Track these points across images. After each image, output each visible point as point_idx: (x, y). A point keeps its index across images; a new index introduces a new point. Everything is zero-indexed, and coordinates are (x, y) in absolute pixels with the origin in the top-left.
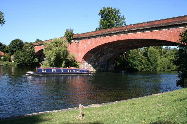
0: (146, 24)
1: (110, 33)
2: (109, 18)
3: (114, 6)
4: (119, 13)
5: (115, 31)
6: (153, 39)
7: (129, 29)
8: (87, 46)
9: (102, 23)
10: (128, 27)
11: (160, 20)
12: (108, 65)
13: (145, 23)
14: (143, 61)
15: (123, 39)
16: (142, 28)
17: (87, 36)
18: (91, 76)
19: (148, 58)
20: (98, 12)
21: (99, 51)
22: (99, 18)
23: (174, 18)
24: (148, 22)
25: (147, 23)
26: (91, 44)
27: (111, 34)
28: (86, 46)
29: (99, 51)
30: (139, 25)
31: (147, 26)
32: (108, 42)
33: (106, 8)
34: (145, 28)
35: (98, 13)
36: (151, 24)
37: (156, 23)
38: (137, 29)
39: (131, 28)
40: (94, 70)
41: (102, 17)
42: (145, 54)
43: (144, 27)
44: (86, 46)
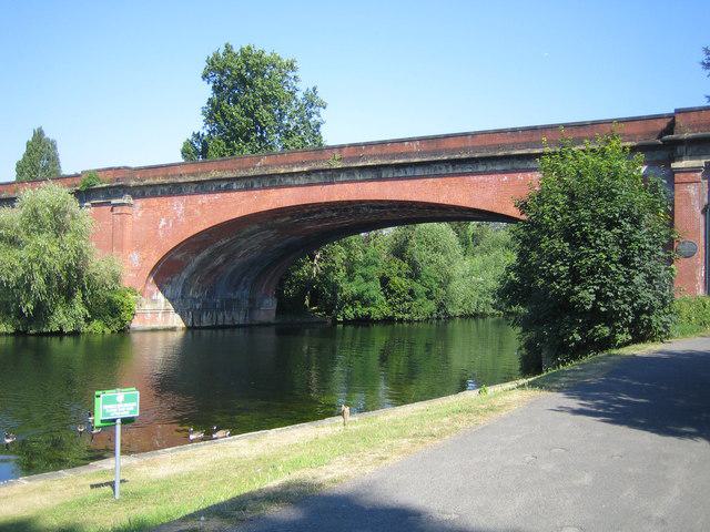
0: (415, 147)
1: (271, 171)
2: (246, 100)
3: (268, 41)
4: (291, 74)
5: (294, 164)
6: (441, 202)
7: (352, 159)
8: (167, 221)
9: (214, 112)
10: (345, 150)
11: (466, 134)
12: (252, 301)
13: (411, 140)
14: (571, 157)
15: (325, 200)
16: (401, 161)
17: (171, 180)
18: (334, 294)
19: (413, 265)
20: (202, 66)
21: (219, 244)
22: (206, 91)
23: (514, 131)
24: (421, 139)
25: (418, 143)
26: (189, 213)
27: (272, 181)
28: (163, 223)
29: (219, 244)
30: (389, 149)
31: (420, 154)
32: (264, 208)
33: (236, 50)
34: (412, 160)
35: (201, 71)
36: (433, 147)
37: (452, 144)
38: (379, 162)
39: (359, 158)
40: (176, 321)
41: (217, 89)
42: (399, 251)
43: (407, 155)
44: (163, 223)
